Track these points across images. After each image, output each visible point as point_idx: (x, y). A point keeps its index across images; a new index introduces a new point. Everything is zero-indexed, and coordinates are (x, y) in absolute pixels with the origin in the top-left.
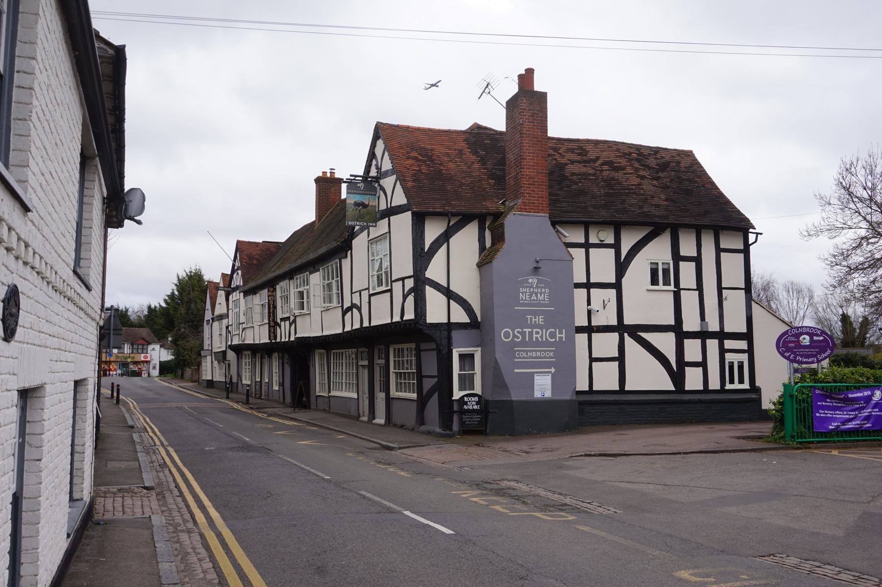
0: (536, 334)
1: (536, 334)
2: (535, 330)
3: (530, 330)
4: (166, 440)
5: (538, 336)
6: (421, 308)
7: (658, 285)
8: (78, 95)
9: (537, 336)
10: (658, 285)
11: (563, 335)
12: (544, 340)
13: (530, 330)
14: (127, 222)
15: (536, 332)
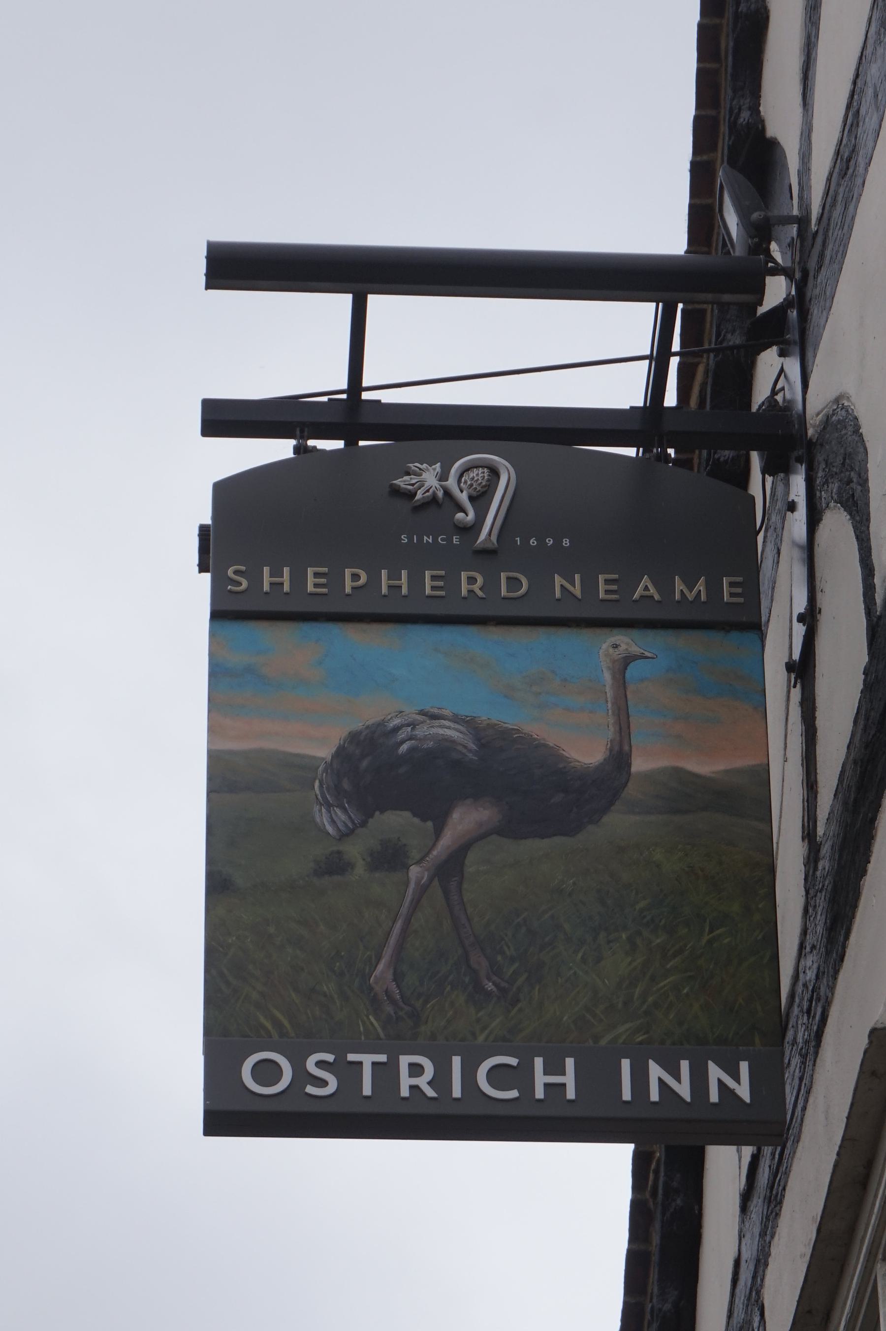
0: (411, 1075)
1: (411, 1075)
2: (405, 1061)
3: (382, 1058)
4: (723, 580)
5: (422, 1082)
6: (834, 860)
7: (545, 1073)
8: (806, 360)
9: (415, 1081)
10: (545, 1073)
11: (569, 1079)
12: (457, 1092)
13: (382, 1058)
14: (772, 477)
15: (411, 1065)
